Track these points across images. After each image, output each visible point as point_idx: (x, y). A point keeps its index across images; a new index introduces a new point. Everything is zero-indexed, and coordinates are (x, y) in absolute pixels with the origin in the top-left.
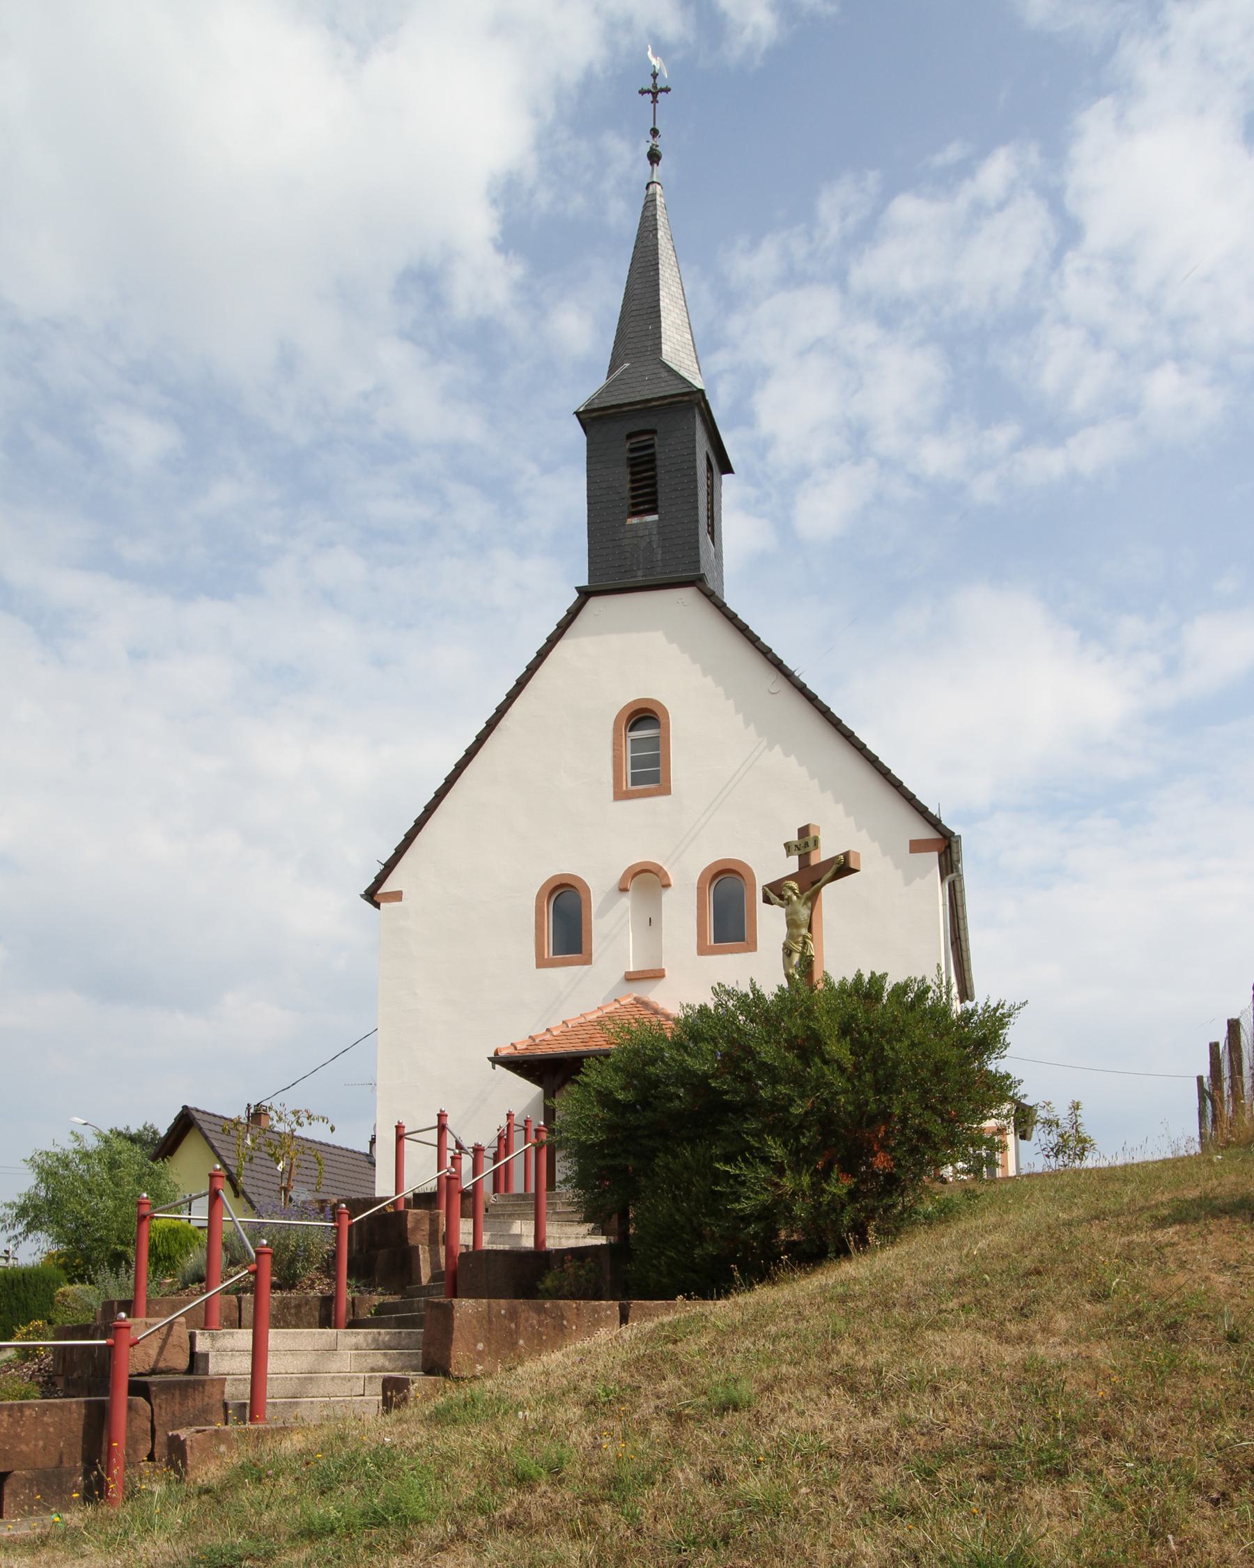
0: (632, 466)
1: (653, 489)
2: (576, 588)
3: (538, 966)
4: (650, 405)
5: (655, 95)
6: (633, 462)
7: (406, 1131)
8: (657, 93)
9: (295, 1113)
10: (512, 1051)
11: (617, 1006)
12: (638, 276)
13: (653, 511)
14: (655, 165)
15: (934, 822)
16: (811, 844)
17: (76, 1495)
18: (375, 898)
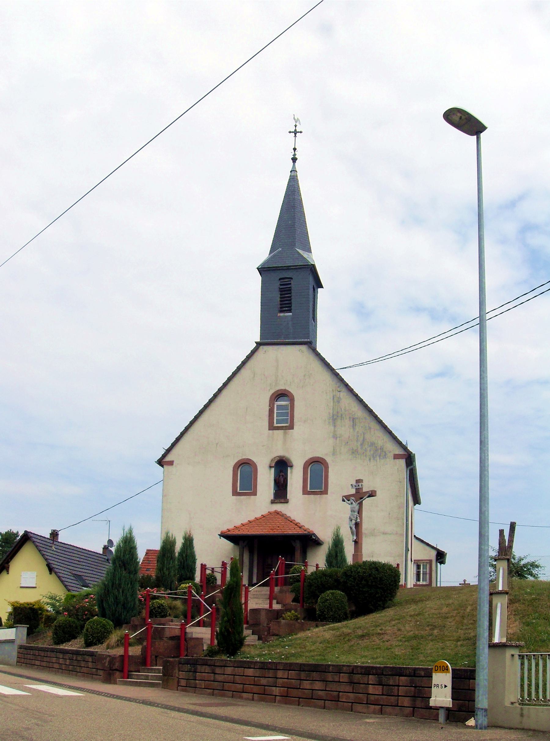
1: (290, 305)
5: (295, 134)
8: (296, 133)
13: (290, 311)
15: (405, 448)
17: (168, 664)
18: (161, 463)
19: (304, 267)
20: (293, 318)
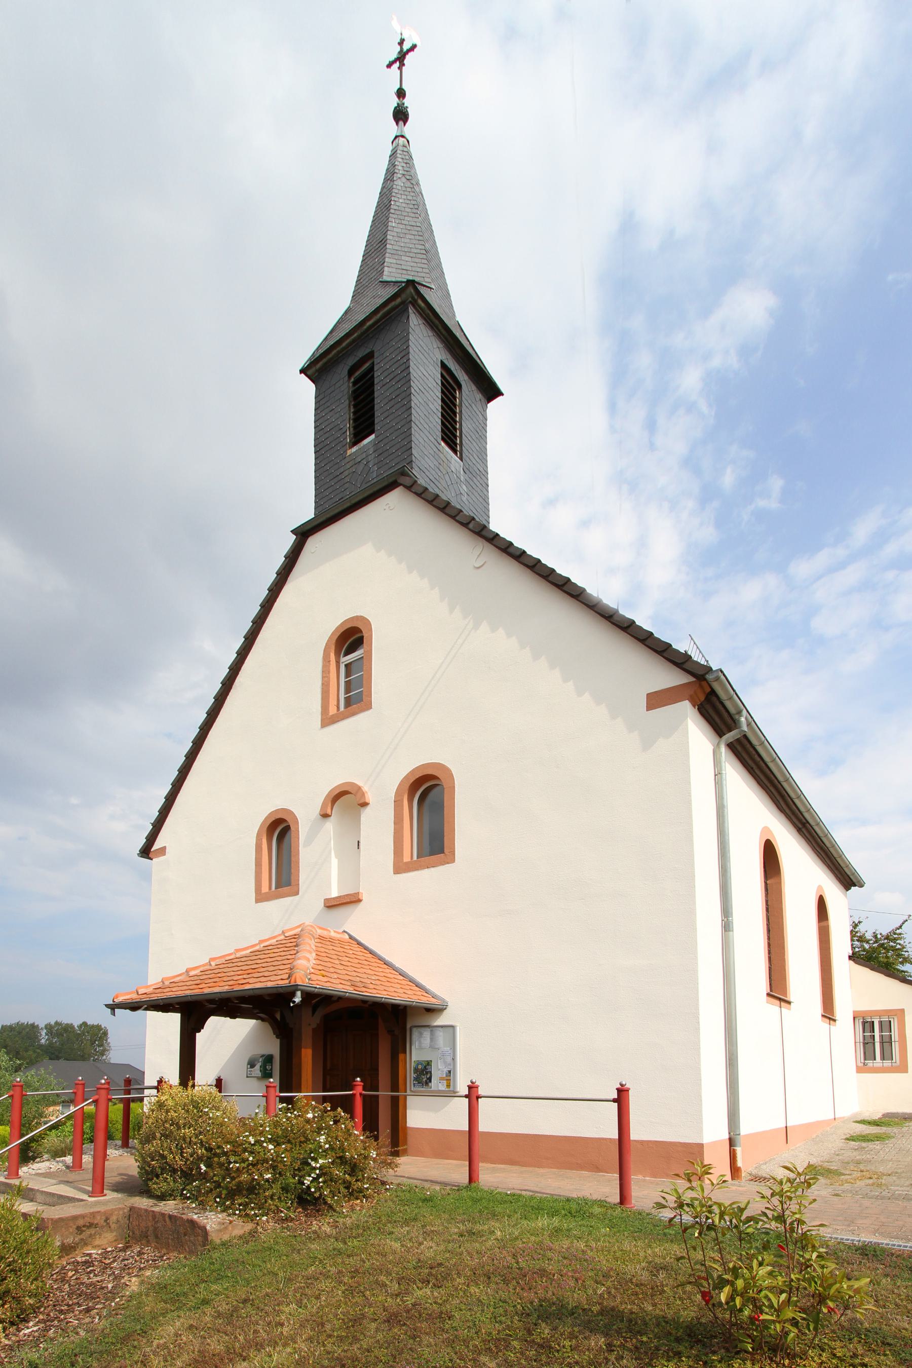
2: (292, 531)
6: (723, 727)
14: (401, 123)
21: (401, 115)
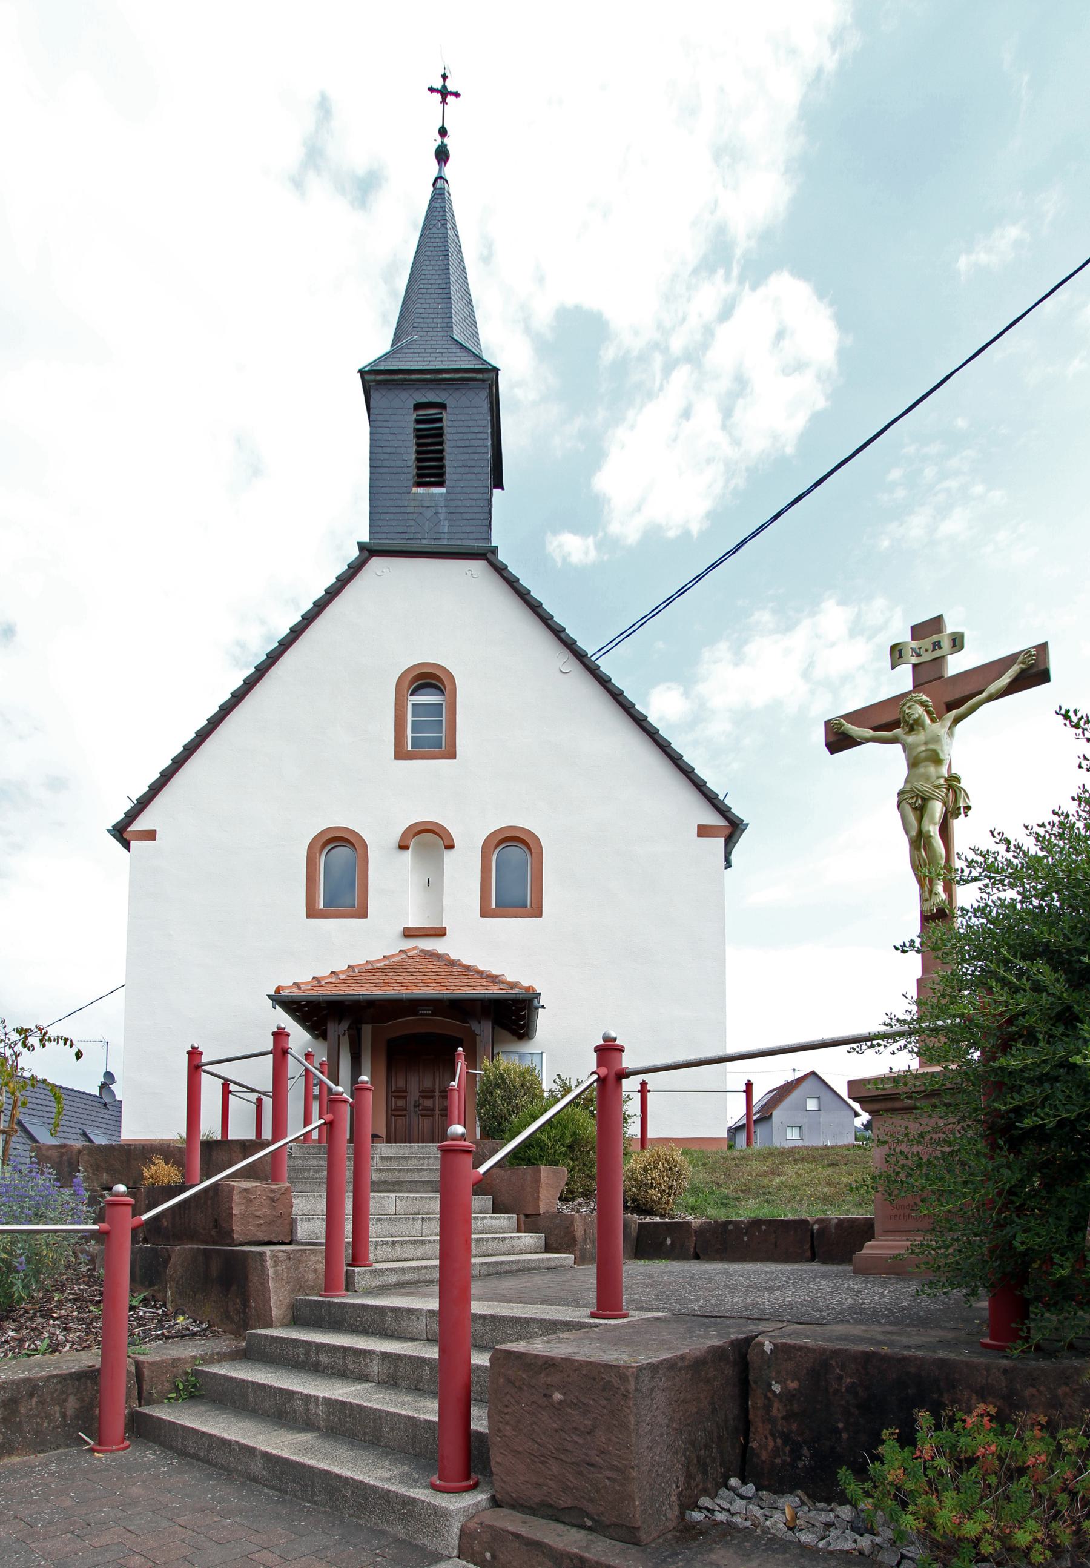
0: (418, 437)
2: (358, 543)
3: (309, 916)
4: (440, 376)
7: (204, 1059)
9: (21, 1031)
10: (295, 990)
11: (404, 956)
12: (426, 258)
13: (441, 484)
15: (722, 809)
16: (946, 644)
19: (474, 375)
20: (448, 499)
21: (442, 155)
